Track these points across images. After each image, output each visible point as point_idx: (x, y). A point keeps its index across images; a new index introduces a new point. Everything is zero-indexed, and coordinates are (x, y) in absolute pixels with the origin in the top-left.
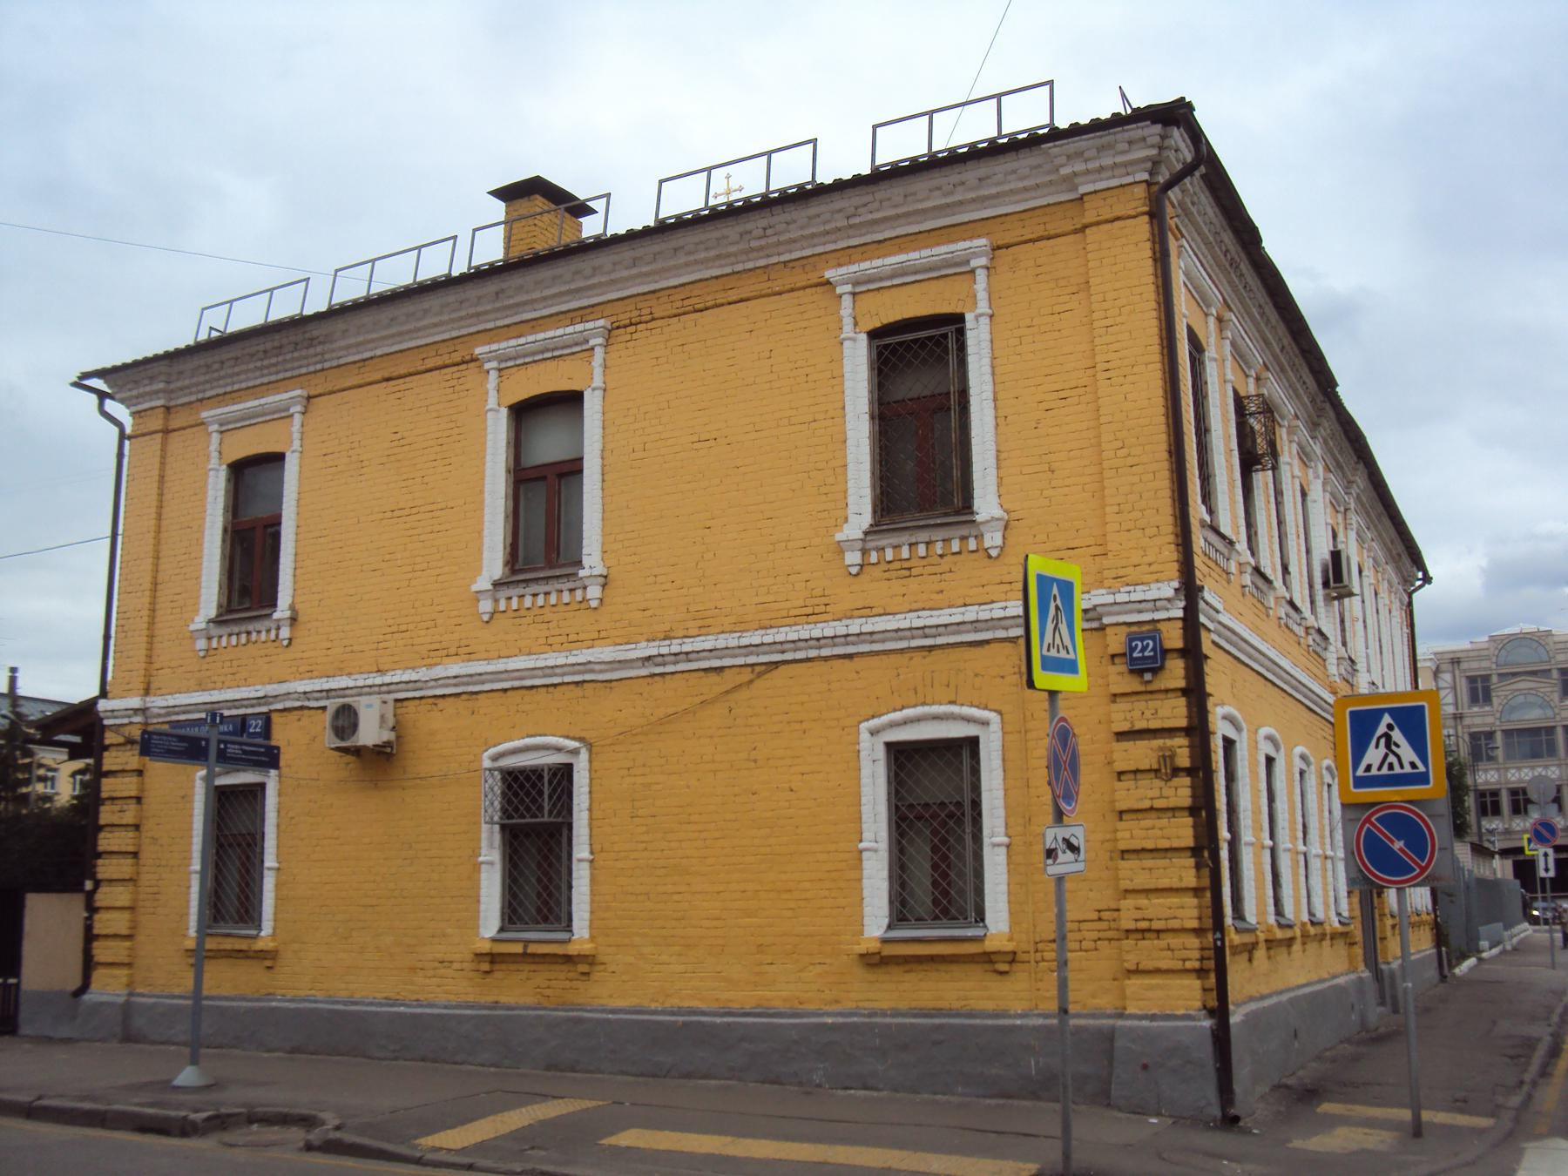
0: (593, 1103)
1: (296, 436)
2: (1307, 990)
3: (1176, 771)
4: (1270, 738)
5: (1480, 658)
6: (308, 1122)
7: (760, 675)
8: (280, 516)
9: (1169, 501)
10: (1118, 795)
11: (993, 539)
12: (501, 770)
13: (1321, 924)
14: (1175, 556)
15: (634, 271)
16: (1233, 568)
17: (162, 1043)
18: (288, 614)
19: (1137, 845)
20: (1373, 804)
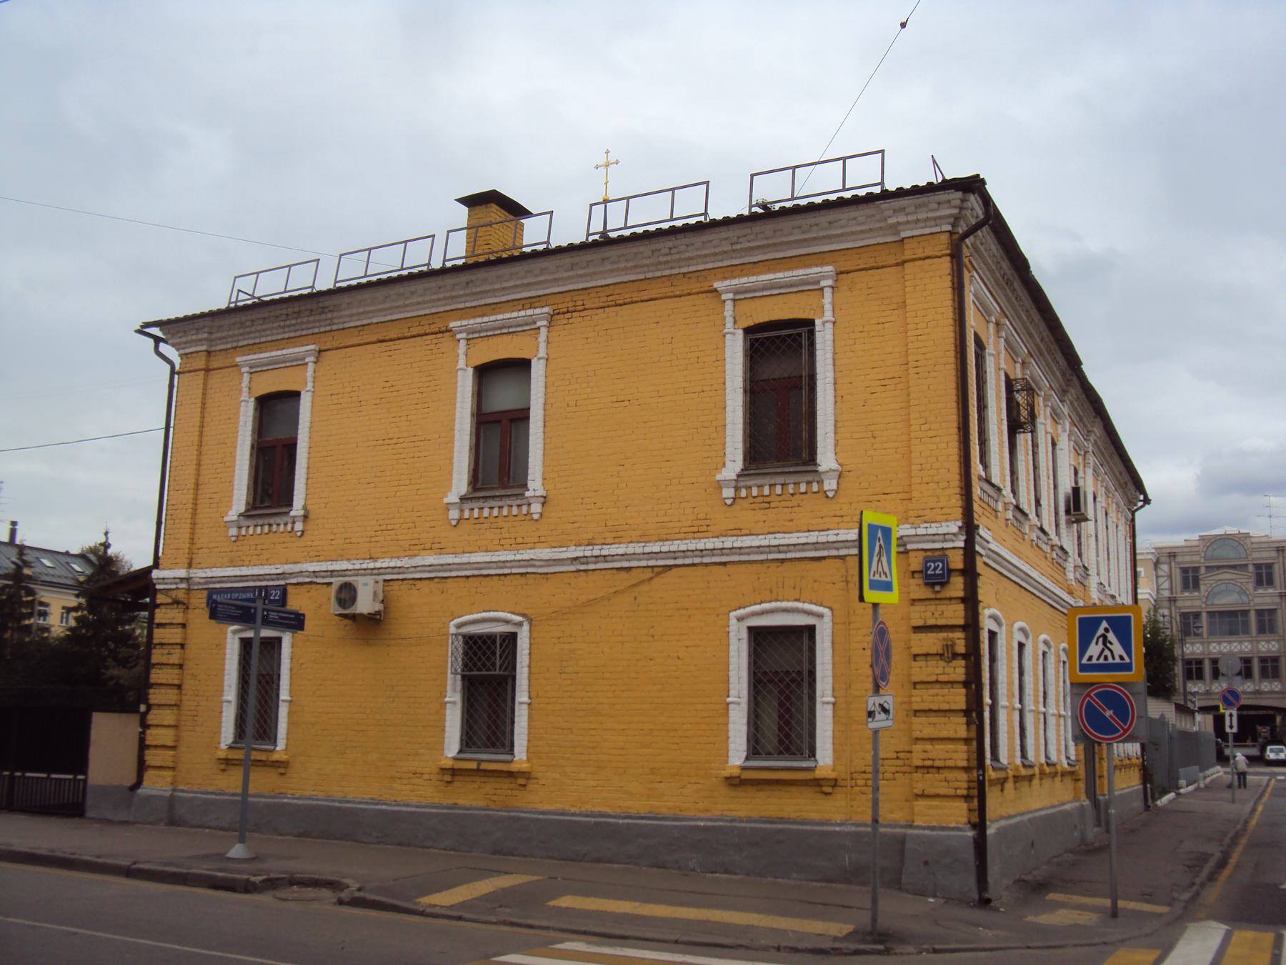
0: (535, 878)
1: (310, 379)
2: (1043, 813)
3: (955, 656)
4: (1022, 630)
5: (1191, 553)
6: (333, 885)
7: (658, 574)
8: (296, 439)
9: (957, 464)
10: (913, 671)
11: (830, 484)
12: (464, 636)
13: (1054, 765)
14: (960, 503)
15: (571, 273)
16: (1000, 508)
17: (198, 827)
18: (302, 513)
19: (926, 706)
20: (1092, 684)
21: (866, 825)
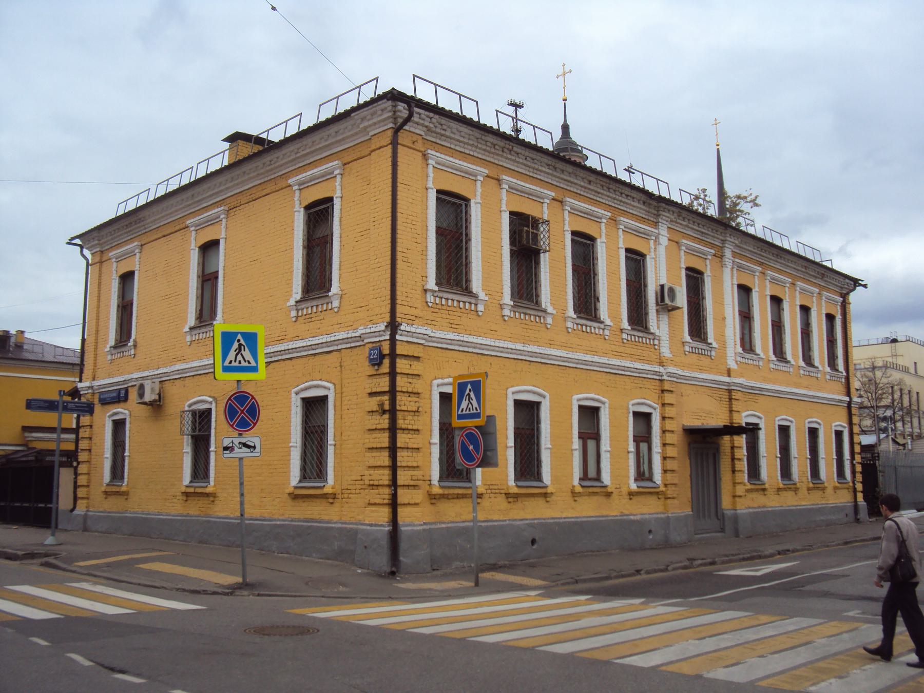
3: (384, 412)
20: (463, 428)
21: (382, 525)
